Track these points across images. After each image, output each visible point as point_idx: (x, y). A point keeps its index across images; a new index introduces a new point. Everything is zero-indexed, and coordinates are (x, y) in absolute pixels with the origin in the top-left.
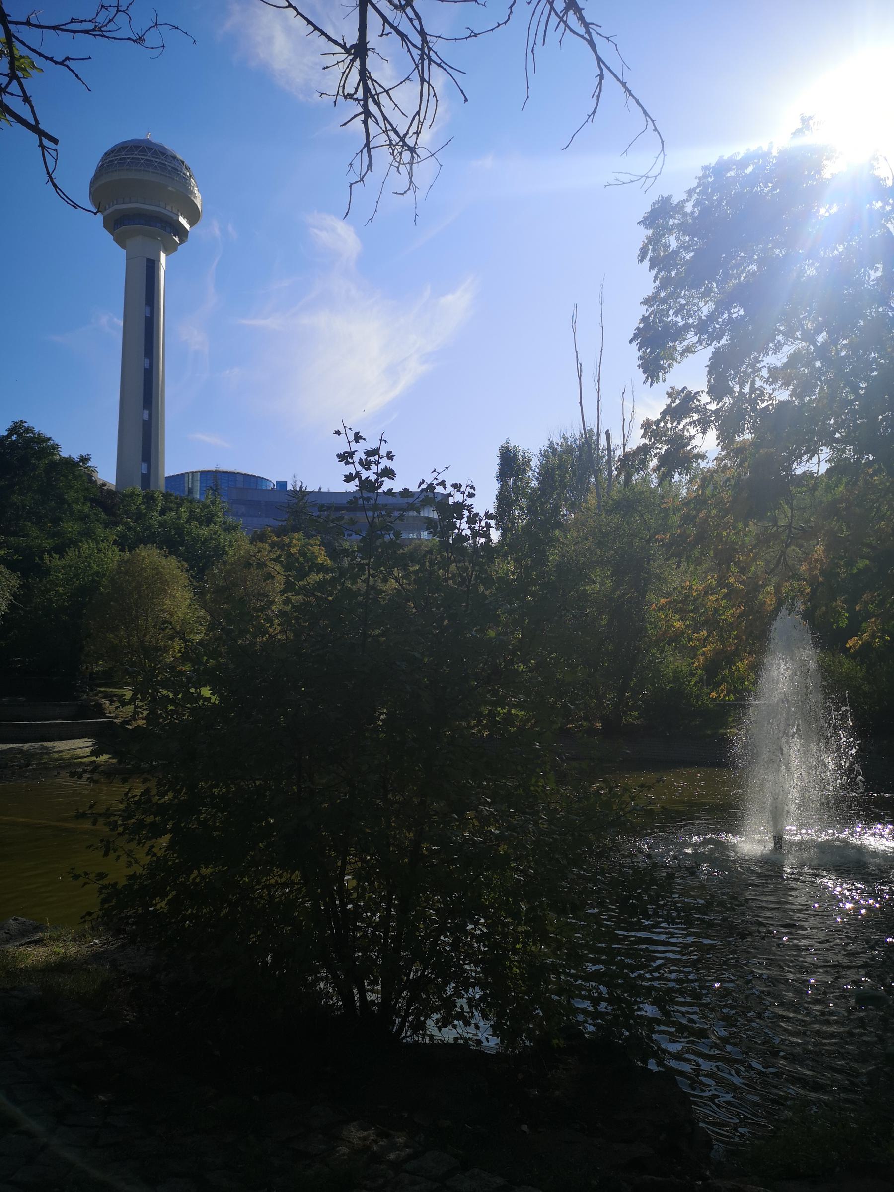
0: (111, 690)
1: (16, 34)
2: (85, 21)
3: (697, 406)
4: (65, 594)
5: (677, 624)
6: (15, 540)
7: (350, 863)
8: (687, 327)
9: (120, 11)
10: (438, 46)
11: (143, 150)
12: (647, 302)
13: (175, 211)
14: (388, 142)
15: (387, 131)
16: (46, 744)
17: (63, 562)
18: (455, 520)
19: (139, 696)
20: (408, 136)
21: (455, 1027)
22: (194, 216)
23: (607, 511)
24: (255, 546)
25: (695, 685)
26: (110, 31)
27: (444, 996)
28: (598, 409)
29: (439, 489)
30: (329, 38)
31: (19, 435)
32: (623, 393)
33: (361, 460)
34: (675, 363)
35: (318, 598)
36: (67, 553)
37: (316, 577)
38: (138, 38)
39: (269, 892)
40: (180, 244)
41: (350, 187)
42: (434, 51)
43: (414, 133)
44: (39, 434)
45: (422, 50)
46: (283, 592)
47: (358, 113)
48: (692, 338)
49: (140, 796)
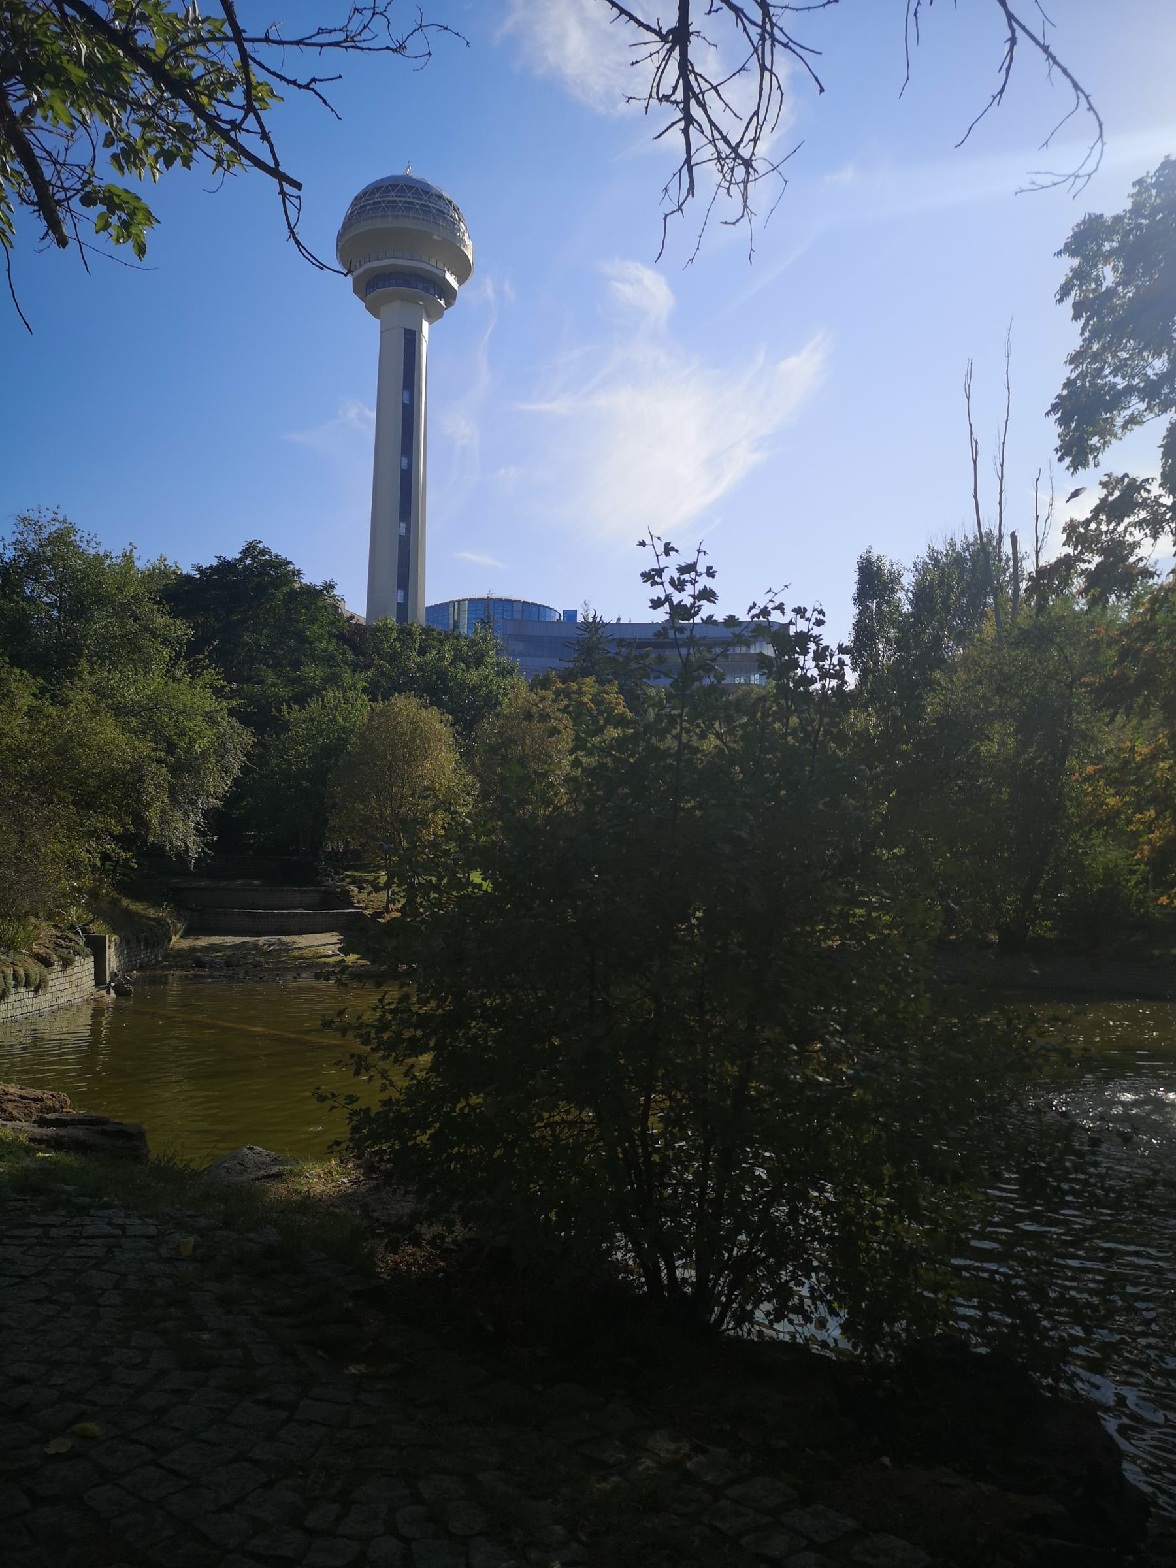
0: (359, 874)
1: (253, 55)
2: (335, 30)
3: (1145, 499)
4: (306, 754)
5: (1111, 801)
6: (248, 688)
7: (656, 1101)
8: (1129, 390)
9: (377, 13)
10: (785, 21)
11: (402, 190)
12: (1075, 359)
13: (440, 265)
14: (716, 156)
15: (714, 140)
16: (284, 938)
17: (304, 714)
18: (797, 656)
19: (395, 880)
20: (742, 145)
21: (791, 1322)
22: (464, 270)
23: (1010, 644)
24: (536, 694)
25: (1136, 886)
26: (364, 41)
27: (778, 1281)
28: (1000, 503)
29: (776, 617)
30: (640, 24)
31: (254, 558)
32: (1037, 480)
33: (672, 579)
34: (1114, 441)
35: (615, 759)
36: (308, 703)
37: (614, 732)
38: (398, 45)
39: (553, 1131)
40: (446, 309)
41: (665, 219)
42: (779, 28)
43: (750, 141)
44: (277, 556)
45: (763, 27)
46: (571, 752)
47: (677, 119)
48: (1136, 405)
49: (398, 1003)
